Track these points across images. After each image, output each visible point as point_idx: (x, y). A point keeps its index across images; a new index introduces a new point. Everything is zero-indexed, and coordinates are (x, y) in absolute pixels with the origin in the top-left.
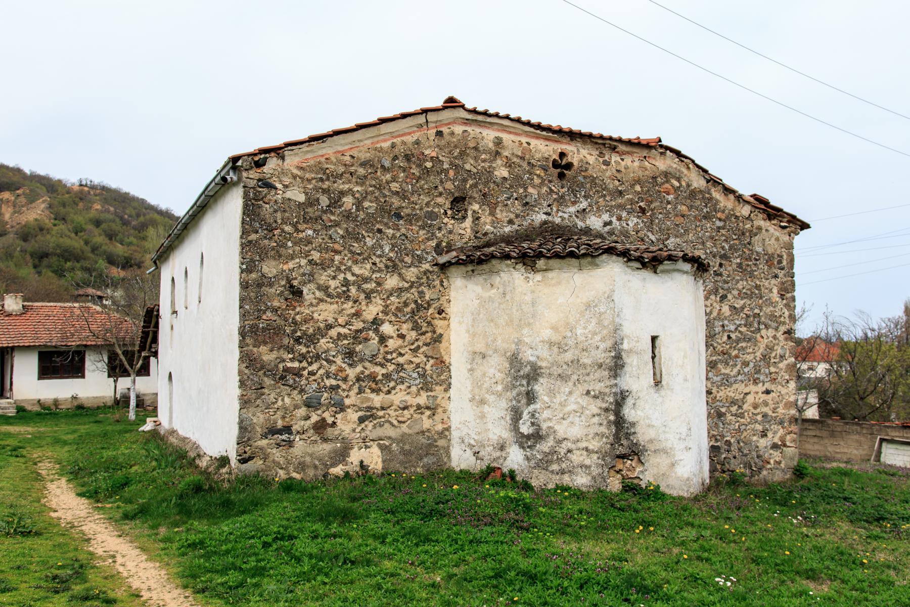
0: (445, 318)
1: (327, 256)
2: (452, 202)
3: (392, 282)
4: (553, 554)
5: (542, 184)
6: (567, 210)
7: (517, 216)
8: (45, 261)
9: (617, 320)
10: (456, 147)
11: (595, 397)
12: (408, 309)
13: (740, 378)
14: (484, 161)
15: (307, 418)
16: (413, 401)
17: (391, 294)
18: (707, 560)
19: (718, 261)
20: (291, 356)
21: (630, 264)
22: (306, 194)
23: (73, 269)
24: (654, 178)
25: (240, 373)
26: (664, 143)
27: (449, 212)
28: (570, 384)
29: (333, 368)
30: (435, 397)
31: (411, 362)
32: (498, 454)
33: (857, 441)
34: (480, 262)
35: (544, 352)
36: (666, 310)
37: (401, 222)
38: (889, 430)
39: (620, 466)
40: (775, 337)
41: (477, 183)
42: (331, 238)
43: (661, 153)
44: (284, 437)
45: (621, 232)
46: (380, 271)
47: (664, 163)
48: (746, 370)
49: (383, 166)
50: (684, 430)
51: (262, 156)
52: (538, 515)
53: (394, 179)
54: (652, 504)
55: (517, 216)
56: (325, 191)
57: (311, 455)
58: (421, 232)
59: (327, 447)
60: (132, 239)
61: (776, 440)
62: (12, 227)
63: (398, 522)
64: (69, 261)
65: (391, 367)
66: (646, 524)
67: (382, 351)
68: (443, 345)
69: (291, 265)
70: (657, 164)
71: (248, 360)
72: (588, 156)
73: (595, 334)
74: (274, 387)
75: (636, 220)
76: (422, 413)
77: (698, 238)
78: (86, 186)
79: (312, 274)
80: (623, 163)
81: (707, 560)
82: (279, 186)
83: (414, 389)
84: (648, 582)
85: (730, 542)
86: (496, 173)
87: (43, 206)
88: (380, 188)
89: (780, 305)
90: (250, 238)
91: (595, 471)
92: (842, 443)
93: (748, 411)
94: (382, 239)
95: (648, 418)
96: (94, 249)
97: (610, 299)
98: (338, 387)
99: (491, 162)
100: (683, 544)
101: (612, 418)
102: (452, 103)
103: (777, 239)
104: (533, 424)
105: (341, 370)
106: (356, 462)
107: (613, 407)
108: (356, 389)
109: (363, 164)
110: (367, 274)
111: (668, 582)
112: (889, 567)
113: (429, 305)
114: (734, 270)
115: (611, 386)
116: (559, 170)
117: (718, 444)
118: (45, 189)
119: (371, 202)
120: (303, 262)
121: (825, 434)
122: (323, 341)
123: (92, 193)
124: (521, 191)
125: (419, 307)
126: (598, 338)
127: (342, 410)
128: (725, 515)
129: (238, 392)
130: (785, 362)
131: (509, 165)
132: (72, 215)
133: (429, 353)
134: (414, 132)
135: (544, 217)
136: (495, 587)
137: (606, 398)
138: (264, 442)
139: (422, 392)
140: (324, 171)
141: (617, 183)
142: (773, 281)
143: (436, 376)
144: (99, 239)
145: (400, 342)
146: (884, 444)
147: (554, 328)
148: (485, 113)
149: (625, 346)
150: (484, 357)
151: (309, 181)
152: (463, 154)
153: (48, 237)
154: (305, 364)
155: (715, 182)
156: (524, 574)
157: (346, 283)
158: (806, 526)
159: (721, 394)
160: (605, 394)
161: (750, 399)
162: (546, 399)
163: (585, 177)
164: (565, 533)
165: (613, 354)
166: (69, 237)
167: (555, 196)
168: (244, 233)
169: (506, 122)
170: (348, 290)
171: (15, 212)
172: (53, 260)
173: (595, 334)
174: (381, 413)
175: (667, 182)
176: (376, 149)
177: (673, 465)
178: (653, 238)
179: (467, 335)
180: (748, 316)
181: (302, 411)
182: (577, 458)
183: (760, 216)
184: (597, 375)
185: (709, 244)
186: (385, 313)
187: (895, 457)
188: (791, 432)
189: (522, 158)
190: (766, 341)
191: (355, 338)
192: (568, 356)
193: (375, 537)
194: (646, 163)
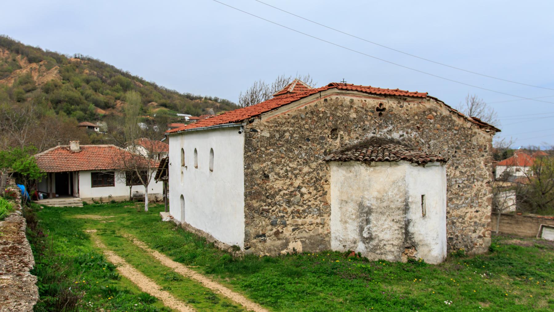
0: (328, 184)
3: (306, 169)
4: (383, 291)
5: (372, 119)
6: (383, 131)
7: (360, 135)
8: (59, 105)
9: (407, 189)
10: (333, 106)
11: (396, 222)
12: (312, 181)
13: (463, 205)
14: (345, 111)
15: (272, 230)
16: (315, 221)
18: (442, 294)
19: (454, 150)
22: (270, 133)
23: (75, 110)
24: (424, 112)
25: (245, 212)
27: (330, 136)
28: (386, 216)
29: (282, 208)
34: (345, 161)
35: (374, 202)
36: (428, 184)
38: (547, 221)
39: (406, 252)
40: (481, 185)
42: (280, 152)
43: (428, 100)
44: (263, 238)
46: (301, 165)
47: (428, 105)
48: (467, 201)
49: (301, 118)
50: (435, 236)
52: (374, 274)
53: (306, 123)
54: (421, 269)
55: (360, 135)
57: (273, 246)
58: (318, 146)
59: (279, 243)
60: (108, 91)
61: (481, 234)
62: (39, 85)
63: (319, 277)
65: (306, 207)
66: (418, 278)
67: (302, 199)
68: (327, 196)
69: (264, 165)
70: (426, 105)
71: (248, 206)
72: (393, 104)
73: (397, 195)
74: (259, 217)
75: (415, 133)
78: (79, 58)
79: (273, 168)
80: (409, 106)
81: (442, 294)
82: (259, 131)
83: (315, 216)
84: (419, 303)
85: (453, 286)
87: (56, 72)
88: (300, 128)
89: (485, 170)
92: (522, 227)
93: (467, 221)
96: (87, 98)
97: (404, 179)
98: (284, 216)
99: (348, 111)
100: (433, 287)
101: (404, 231)
103: (484, 138)
104: (369, 233)
105: (285, 209)
106: (292, 248)
107: (404, 227)
108: (291, 217)
109: (293, 118)
110: (295, 166)
111: (426, 303)
112: (516, 297)
113: (321, 178)
117: (452, 236)
118: (55, 61)
120: (269, 163)
121: (513, 222)
122: (277, 197)
123: (82, 62)
124: (362, 123)
125: (317, 180)
126: (398, 197)
128: (452, 273)
129: (244, 220)
130: (486, 197)
131: (357, 112)
133: (322, 200)
135: (372, 135)
136: (363, 304)
138: (255, 241)
140: (277, 122)
141: (406, 116)
142: (482, 158)
143: (324, 210)
144: (89, 91)
145: (309, 195)
146: (544, 228)
147: (379, 192)
149: (410, 200)
150: (347, 202)
151: (271, 127)
153: (60, 90)
154: (270, 207)
155: (453, 112)
156: (374, 299)
157: (287, 171)
158: (487, 278)
159: (454, 213)
160: (401, 221)
161: (468, 215)
162: (375, 222)
163: (391, 114)
164: (385, 282)
167: (377, 125)
168: (246, 152)
171: (40, 76)
173: (397, 195)
174: (301, 227)
175: (431, 113)
176: (298, 110)
178: (423, 141)
180: (468, 176)
181: (269, 227)
182: (388, 248)
183: (476, 127)
184: (397, 213)
185: (450, 142)
186: (303, 183)
187: (549, 235)
188: (487, 230)
189: (363, 108)
190: (477, 187)
191: (290, 195)
192: (385, 204)
193: (313, 284)
194: (421, 105)
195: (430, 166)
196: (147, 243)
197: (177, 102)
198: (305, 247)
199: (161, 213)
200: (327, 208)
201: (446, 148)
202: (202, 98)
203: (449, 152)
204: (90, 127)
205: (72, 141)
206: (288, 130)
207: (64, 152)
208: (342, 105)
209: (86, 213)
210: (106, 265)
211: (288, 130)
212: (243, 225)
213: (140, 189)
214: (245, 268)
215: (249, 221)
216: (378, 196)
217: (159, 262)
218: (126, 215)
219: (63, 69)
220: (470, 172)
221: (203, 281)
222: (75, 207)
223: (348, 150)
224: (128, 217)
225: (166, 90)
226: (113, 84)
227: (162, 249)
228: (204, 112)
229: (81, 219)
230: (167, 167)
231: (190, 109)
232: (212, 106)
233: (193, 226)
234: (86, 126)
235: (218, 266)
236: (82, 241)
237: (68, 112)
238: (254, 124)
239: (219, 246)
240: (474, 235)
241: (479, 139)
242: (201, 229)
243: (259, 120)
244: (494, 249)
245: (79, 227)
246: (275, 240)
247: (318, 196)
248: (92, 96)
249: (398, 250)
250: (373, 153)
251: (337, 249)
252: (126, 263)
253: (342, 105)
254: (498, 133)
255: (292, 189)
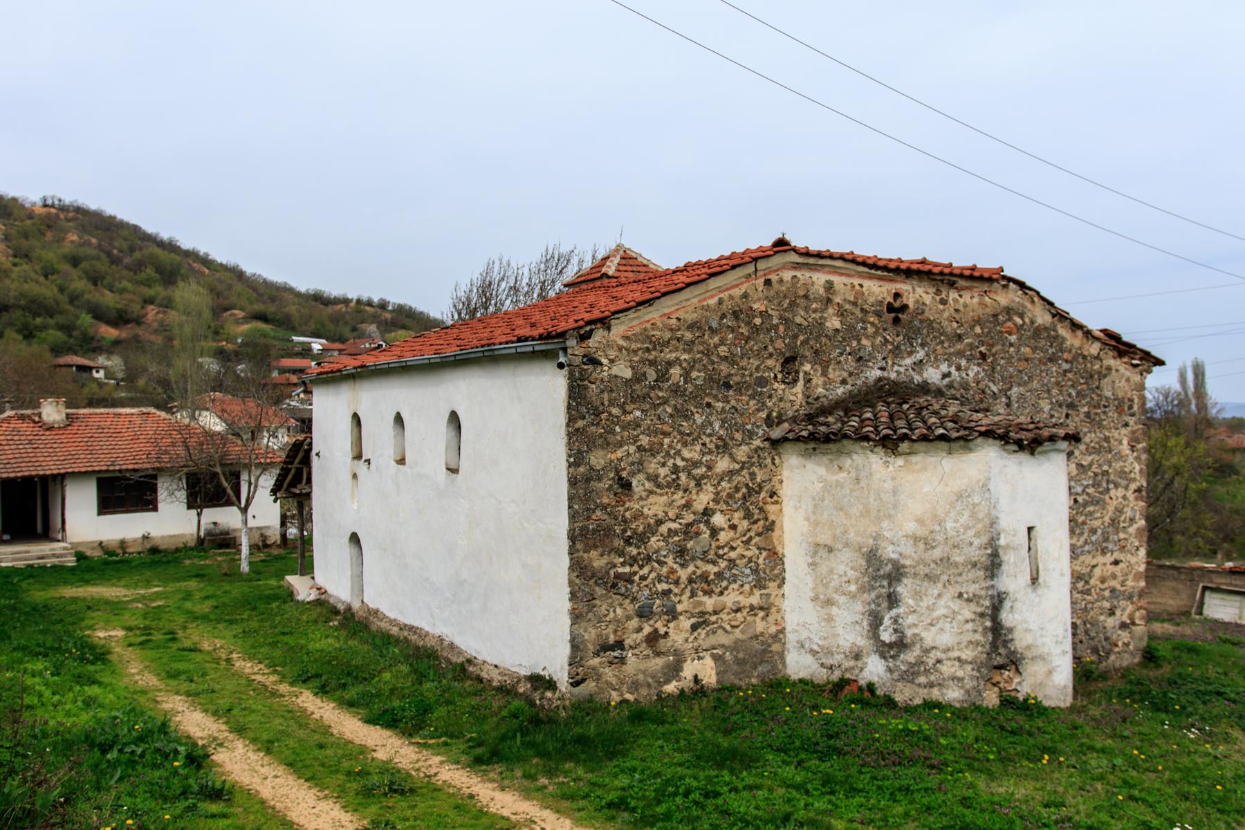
0: (777, 502)
1: (656, 440)
2: (782, 365)
3: (723, 464)
5: (876, 333)
6: (903, 363)
9: (994, 512)
10: (785, 297)
11: (969, 600)
13: (1087, 548)
14: (815, 311)
15: (640, 630)
16: (746, 601)
17: (722, 479)
19: (1065, 410)
20: (622, 560)
21: (1007, 447)
22: (633, 368)
23: (45, 327)
24: (995, 316)
25: (571, 583)
26: (1007, 273)
27: (780, 376)
28: (940, 585)
29: (665, 570)
30: (768, 595)
31: (744, 556)
32: (852, 663)
33: (1173, 589)
36: (1029, 495)
37: (731, 392)
38: (1213, 576)
39: (997, 678)
40: (1124, 498)
41: (808, 339)
42: (659, 418)
43: (1004, 286)
45: (960, 383)
47: (1005, 298)
48: (1093, 538)
49: (710, 328)
51: (588, 328)
53: (722, 342)
55: (851, 374)
56: (653, 363)
57: (644, 672)
58: (752, 403)
59: (659, 662)
60: (125, 283)
61: (1125, 619)
64: (39, 316)
65: (723, 564)
66: (1053, 752)
67: (713, 546)
68: (776, 534)
69: (619, 454)
70: (998, 298)
71: (579, 568)
72: (924, 295)
73: (967, 528)
74: (606, 597)
75: (976, 369)
76: (755, 615)
77: (1043, 385)
78: (53, 206)
80: (961, 301)
82: (605, 361)
83: (747, 587)
86: (828, 324)
89: (1131, 459)
90: (577, 426)
91: (969, 684)
92: (1154, 591)
94: (711, 414)
95: (1026, 622)
96: (73, 299)
97: (985, 488)
99: (822, 311)
101: (988, 624)
102: (781, 244)
103: (1128, 380)
104: (896, 631)
105: (673, 571)
107: (989, 612)
108: (688, 594)
109: (690, 327)
110: (696, 456)
113: (760, 487)
114: (1082, 421)
115: (987, 588)
116: (893, 315)
119: (699, 371)
120: (632, 449)
123: (62, 216)
124: (854, 343)
126: (971, 533)
127: (675, 618)
129: (568, 605)
130: (1135, 526)
131: (841, 313)
132: (38, 250)
134: (742, 283)
135: (879, 373)
137: (982, 602)
138: (597, 661)
139: (755, 590)
142: (1124, 431)
143: (769, 571)
145: (731, 534)
146: (1207, 594)
147: (920, 521)
148: (819, 255)
149: (1002, 542)
150: (831, 550)
151: (635, 352)
152: (793, 304)
153: (7, 282)
154: (636, 568)
160: (980, 597)
161: (1097, 572)
162: (911, 602)
163: (921, 321)
165: (989, 551)
166: (37, 282)
167: (890, 347)
168: (571, 420)
169: (839, 263)
170: (678, 478)
172: (17, 314)
173: (967, 528)
174: (713, 618)
175: (1010, 319)
177: (1050, 672)
178: (995, 389)
179: (806, 523)
180: (1096, 474)
181: (634, 623)
182: (947, 669)
183: (1111, 353)
184: (971, 575)
185: (1055, 391)
186: (716, 501)
187: (1221, 609)
188: (1139, 608)
189: (855, 304)
190: (1115, 502)
191: (686, 533)
192: (937, 553)
195: (1045, 452)
196: (272, 666)
197: (292, 309)
198: (725, 672)
199: (289, 578)
200: (776, 565)
201: (1046, 407)
202: (351, 301)
203: (1052, 416)
204: (81, 368)
205: (46, 398)
206: (678, 359)
207: (25, 427)
208: (806, 297)
209: (87, 582)
210: (182, 749)
211: (678, 359)
212: (567, 621)
213: (227, 517)
214: (581, 740)
215: (582, 607)
216: (919, 533)
217: (326, 730)
218: (192, 584)
219: (14, 232)
220: (1100, 466)
221: (475, 790)
222: (54, 567)
223: (826, 411)
224: (201, 590)
225: (265, 281)
226: (139, 266)
227: (323, 686)
228: (355, 334)
229: (74, 600)
230: (307, 461)
231: (323, 325)
232: (375, 319)
233: (392, 615)
234: (71, 366)
235: (503, 738)
236: (91, 668)
237: (26, 332)
238: (592, 342)
239: (484, 675)
240: (1111, 622)
241: (1117, 385)
242: (415, 624)
243: (606, 333)
244: (1156, 654)
245: (74, 623)
246: (647, 657)
247: (752, 534)
248: (86, 296)
249: (975, 673)
250: (892, 419)
251: (803, 674)
252: (231, 736)
253: (806, 297)
254: (1156, 369)
255: (689, 518)
